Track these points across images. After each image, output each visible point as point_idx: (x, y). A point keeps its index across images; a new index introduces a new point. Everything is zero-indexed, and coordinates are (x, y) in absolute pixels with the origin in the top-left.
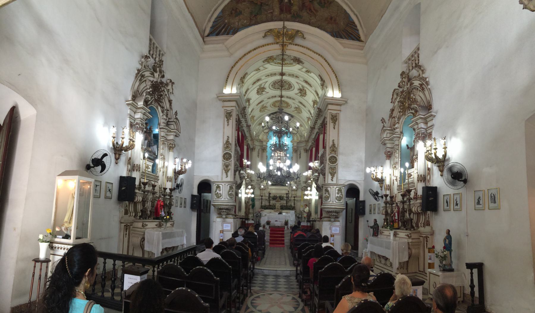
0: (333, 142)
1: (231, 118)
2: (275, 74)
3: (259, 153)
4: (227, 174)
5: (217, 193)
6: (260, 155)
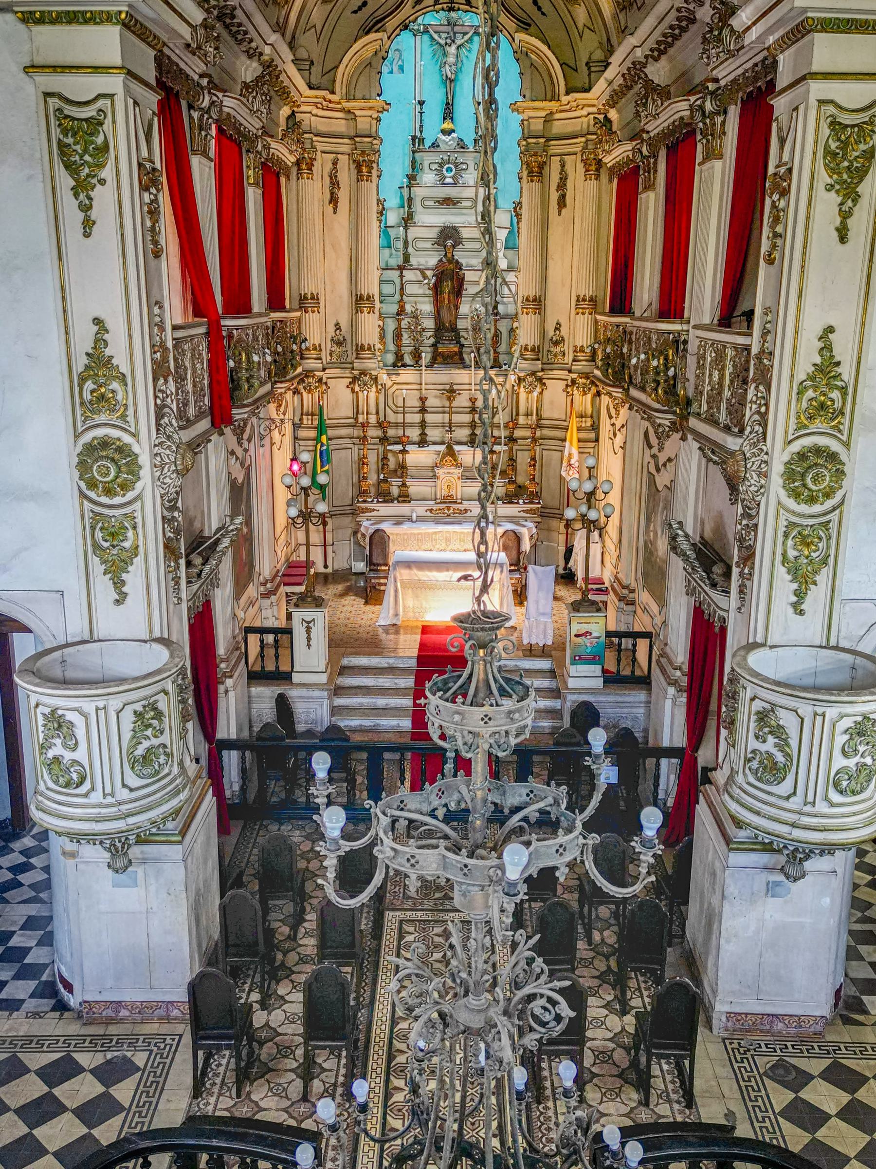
0: (827, 348)
1: (107, 173)
2: (421, 132)
3: (335, 184)
4: (119, 584)
5: (57, 760)
6: (343, 195)
